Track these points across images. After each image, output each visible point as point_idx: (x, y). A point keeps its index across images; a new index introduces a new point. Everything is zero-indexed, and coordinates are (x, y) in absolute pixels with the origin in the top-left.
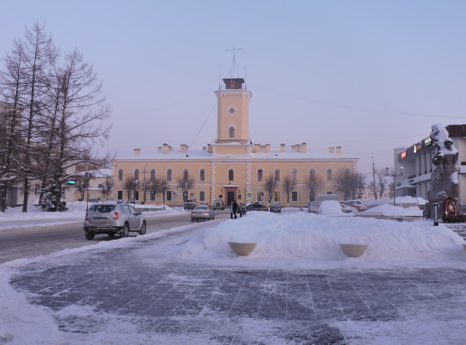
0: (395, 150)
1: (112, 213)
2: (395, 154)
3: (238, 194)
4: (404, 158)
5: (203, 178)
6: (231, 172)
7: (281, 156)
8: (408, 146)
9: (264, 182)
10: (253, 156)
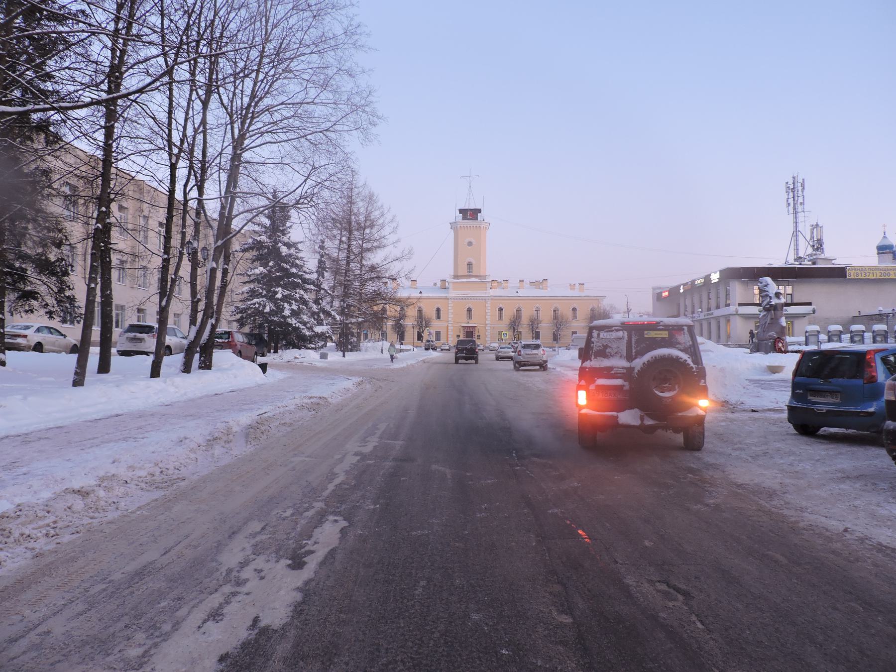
0: (654, 289)
1: (541, 349)
2: (653, 294)
3: (477, 334)
4: (666, 298)
5: (438, 317)
6: (469, 310)
7: (522, 293)
8: (674, 284)
9: (506, 320)
10: (492, 293)
